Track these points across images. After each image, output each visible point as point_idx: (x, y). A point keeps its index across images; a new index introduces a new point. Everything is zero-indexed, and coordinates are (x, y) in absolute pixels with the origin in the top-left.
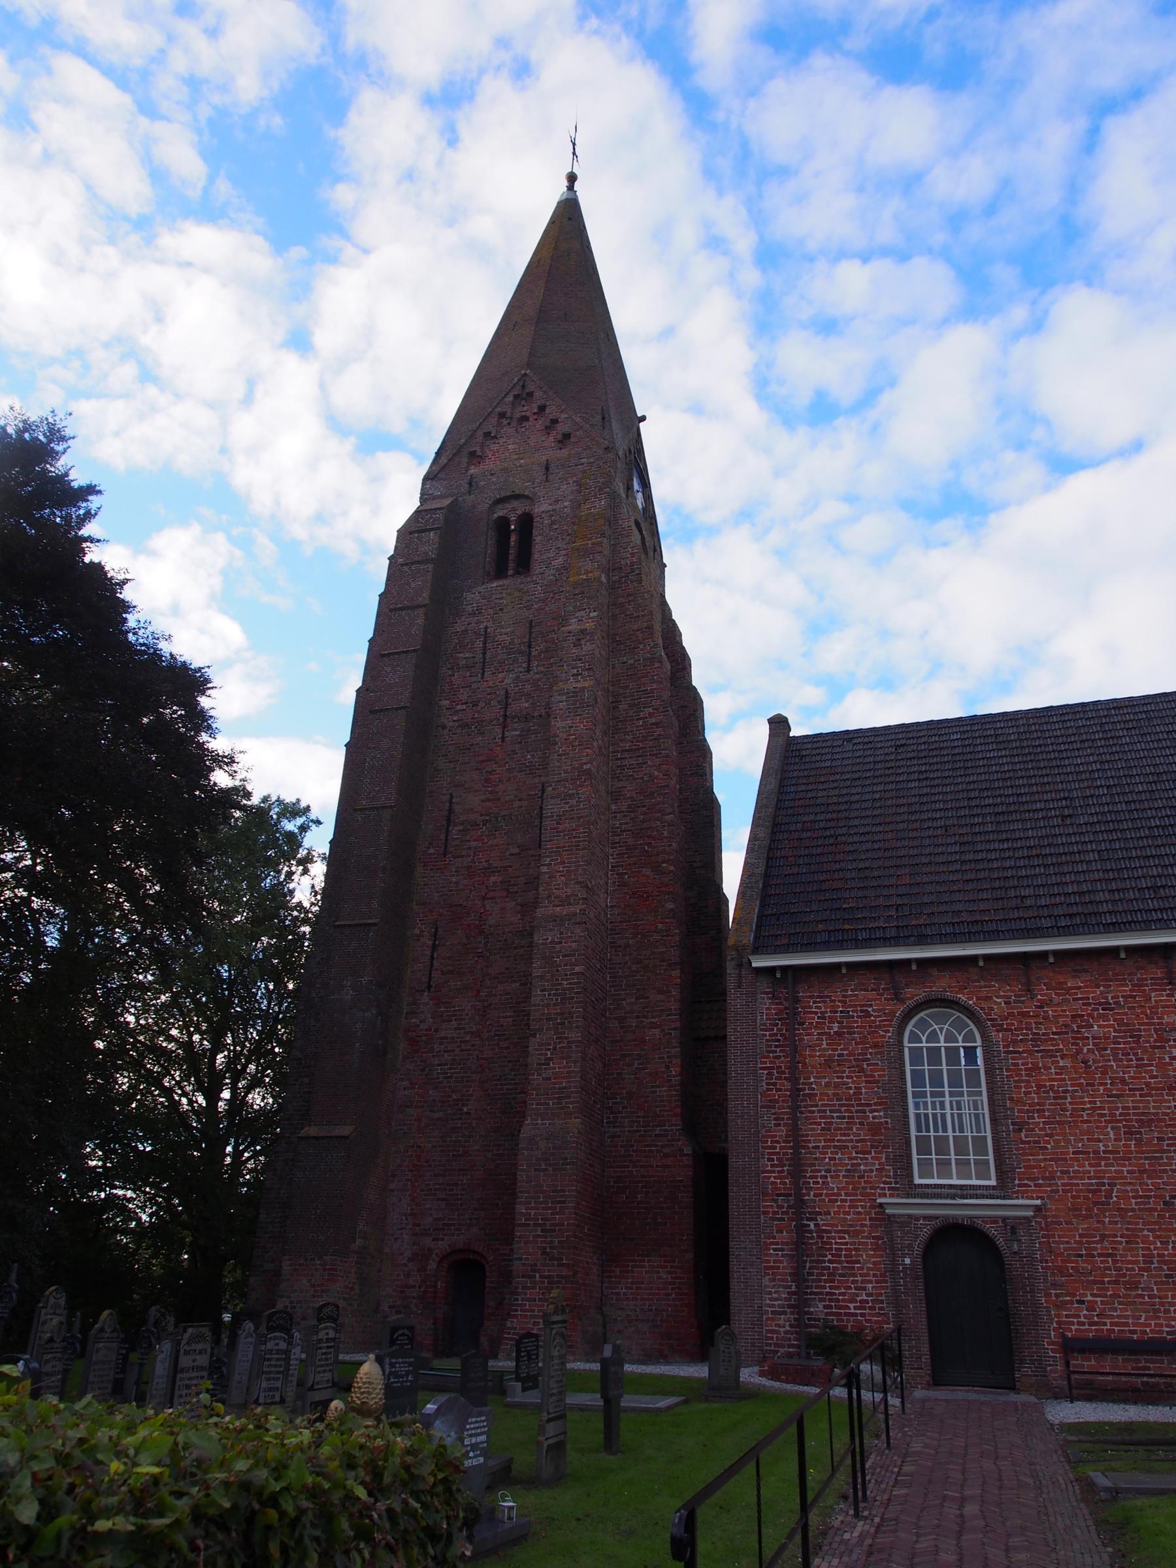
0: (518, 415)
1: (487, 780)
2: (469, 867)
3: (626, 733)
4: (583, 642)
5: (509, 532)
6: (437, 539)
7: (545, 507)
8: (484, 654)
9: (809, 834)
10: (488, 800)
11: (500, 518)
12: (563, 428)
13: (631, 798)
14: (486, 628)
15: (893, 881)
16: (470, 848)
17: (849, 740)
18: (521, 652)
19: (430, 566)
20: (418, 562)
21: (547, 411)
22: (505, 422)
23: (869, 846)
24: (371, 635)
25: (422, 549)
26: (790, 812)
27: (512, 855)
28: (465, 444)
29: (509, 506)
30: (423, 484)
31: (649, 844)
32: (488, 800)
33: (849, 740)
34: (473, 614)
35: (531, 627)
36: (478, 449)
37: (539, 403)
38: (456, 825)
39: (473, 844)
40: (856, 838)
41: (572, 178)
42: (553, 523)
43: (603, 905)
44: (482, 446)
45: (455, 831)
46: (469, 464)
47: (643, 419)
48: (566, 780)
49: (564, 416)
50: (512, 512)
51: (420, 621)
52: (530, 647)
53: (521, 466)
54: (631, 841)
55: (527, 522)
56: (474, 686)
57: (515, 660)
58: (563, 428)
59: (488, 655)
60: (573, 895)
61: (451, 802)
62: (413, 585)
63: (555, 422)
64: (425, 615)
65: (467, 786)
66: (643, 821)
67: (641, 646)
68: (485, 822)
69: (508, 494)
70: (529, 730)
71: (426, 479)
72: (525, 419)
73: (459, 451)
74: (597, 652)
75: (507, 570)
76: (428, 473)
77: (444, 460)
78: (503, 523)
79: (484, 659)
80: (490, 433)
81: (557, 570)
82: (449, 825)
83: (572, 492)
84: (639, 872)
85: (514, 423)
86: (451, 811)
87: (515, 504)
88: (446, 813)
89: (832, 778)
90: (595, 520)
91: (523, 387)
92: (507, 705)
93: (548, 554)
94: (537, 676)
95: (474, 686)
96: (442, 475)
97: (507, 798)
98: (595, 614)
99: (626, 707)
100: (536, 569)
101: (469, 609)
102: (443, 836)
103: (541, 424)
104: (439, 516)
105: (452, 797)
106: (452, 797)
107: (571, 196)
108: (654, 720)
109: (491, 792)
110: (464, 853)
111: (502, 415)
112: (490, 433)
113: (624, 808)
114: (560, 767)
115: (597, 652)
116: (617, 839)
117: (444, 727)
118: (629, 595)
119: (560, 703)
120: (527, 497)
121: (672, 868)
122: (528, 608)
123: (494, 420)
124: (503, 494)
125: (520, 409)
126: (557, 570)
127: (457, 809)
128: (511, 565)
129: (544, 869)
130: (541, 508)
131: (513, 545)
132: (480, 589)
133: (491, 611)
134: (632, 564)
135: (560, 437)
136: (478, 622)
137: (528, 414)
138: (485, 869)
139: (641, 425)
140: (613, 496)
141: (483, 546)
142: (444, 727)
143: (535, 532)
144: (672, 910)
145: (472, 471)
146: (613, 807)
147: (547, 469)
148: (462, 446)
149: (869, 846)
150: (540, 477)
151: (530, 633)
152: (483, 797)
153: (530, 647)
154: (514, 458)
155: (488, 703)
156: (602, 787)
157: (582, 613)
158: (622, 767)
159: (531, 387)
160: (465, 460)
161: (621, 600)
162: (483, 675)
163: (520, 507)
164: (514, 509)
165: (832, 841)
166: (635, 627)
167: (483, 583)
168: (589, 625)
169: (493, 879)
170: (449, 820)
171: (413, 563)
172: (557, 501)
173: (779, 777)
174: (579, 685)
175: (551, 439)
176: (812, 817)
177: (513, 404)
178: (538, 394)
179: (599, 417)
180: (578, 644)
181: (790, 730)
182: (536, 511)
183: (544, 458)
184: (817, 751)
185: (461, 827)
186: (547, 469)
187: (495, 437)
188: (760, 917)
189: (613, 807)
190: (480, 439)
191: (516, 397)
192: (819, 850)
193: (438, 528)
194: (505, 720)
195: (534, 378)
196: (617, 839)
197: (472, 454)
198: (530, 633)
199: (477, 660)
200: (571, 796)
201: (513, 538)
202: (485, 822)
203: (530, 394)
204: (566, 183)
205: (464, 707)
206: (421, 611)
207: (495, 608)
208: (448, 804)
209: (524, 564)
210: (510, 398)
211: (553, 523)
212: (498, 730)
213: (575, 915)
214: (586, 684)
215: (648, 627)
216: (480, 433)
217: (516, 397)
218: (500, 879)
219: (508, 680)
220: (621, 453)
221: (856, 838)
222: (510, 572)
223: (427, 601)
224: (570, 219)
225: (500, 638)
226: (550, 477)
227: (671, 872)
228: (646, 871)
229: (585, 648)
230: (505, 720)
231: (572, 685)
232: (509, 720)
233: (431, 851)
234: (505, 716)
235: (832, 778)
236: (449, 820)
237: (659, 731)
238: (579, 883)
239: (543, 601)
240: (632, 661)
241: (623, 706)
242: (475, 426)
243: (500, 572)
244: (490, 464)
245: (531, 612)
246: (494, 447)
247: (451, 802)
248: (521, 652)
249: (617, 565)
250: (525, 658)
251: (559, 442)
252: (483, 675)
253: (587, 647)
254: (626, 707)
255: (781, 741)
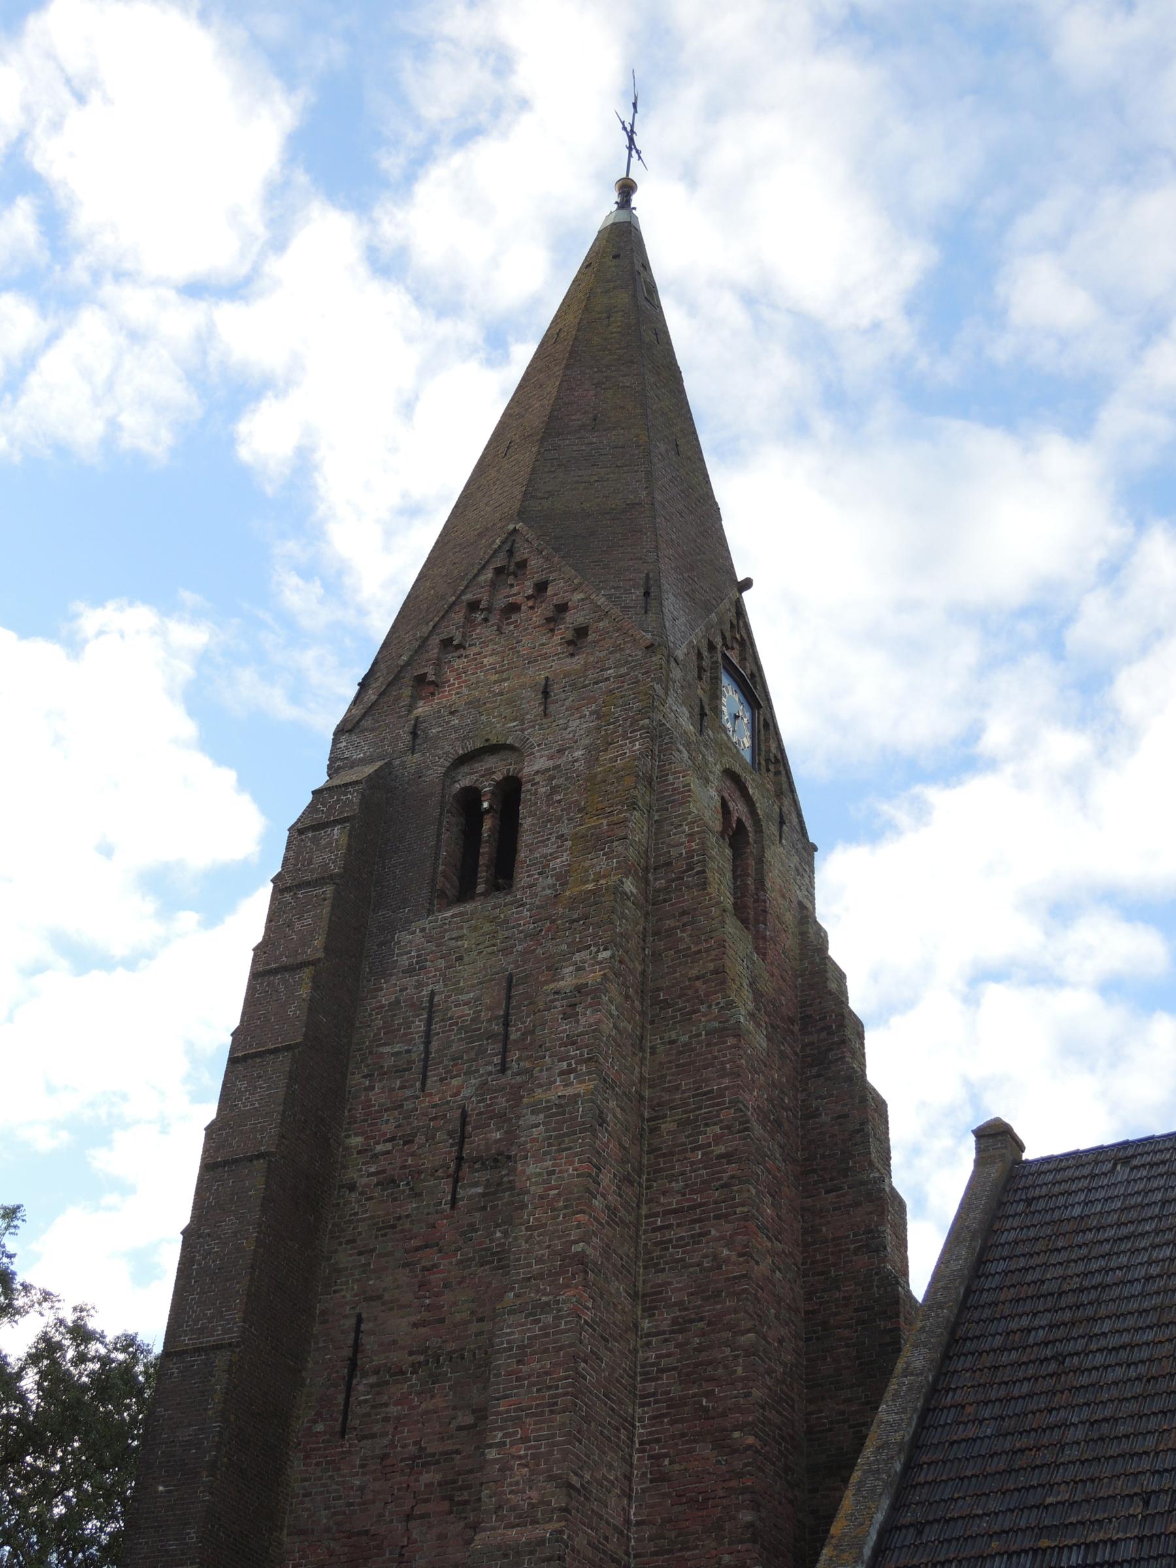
0: (500, 602)
1: (421, 1286)
2: (384, 1457)
3: (672, 1178)
4: (579, 1009)
5: (479, 815)
6: (344, 840)
7: (541, 763)
8: (427, 1043)
9: (1014, 1355)
10: (423, 1323)
11: (465, 790)
12: (574, 618)
13: (680, 1303)
14: (433, 994)
15: (1150, 1443)
16: (386, 1419)
17: (1126, 1161)
18: (491, 1036)
19: (329, 890)
20: (308, 884)
21: (550, 591)
22: (479, 616)
23: (1119, 1372)
24: (235, 1022)
25: (318, 860)
26: (987, 1313)
27: (460, 1428)
28: (407, 664)
29: (481, 766)
30: (335, 741)
31: (709, 1394)
32: (423, 1323)
33: (1126, 1161)
34: (410, 971)
35: (510, 987)
36: (430, 671)
37: (536, 578)
38: (365, 1375)
39: (394, 1410)
40: (1099, 1359)
41: (627, 189)
42: (554, 790)
43: (618, 1521)
44: (438, 664)
45: (362, 1386)
46: (415, 698)
47: (747, 584)
48: (539, 1276)
49: (578, 596)
50: (484, 777)
51: (304, 992)
52: (506, 1024)
53: (501, 694)
54: (676, 1391)
55: (510, 791)
56: (408, 1105)
57: (481, 1052)
58: (574, 618)
59: (435, 1045)
60: (542, 1502)
61: (358, 1331)
62: (298, 926)
63: (562, 608)
64: (314, 979)
65: (387, 1297)
66: (700, 1349)
67: (703, 1008)
68: (416, 1368)
69: (479, 745)
70: (499, 1184)
71: (341, 731)
72: (514, 608)
73: (397, 678)
74: (607, 1027)
75: (475, 885)
76: (344, 721)
77: (371, 696)
78: (471, 797)
79: (427, 1052)
80: (451, 639)
81: (558, 877)
82: (351, 1375)
83: (589, 732)
84: (689, 1451)
85: (494, 619)
86: (356, 1347)
87: (491, 762)
88: (347, 1352)
89: (1079, 1239)
90: (620, 779)
91: (511, 552)
92: (463, 1137)
93: (542, 847)
94: (519, 1079)
95: (408, 1105)
96: (367, 723)
97: (458, 1317)
98: (606, 954)
99: (673, 1126)
100: (522, 878)
101: (404, 961)
102: (340, 1398)
103: (537, 616)
104: (354, 797)
105: (360, 1320)
106: (360, 1320)
107: (623, 216)
108: (721, 1149)
109: (428, 1308)
110: (376, 1428)
111: (473, 606)
112: (451, 639)
113: (665, 1325)
114: (528, 1252)
115: (607, 1027)
116: (651, 1387)
117: (352, 1187)
118: (683, 913)
119: (534, 1128)
120: (511, 748)
121: (751, 1440)
122: (506, 951)
123: (458, 617)
124: (470, 746)
125: (506, 591)
126: (558, 877)
127: (369, 1342)
128: (483, 874)
129: (492, 1454)
130: (536, 764)
131: (484, 836)
132: (425, 923)
133: (442, 963)
134: (691, 853)
135: (569, 635)
136: (419, 985)
137: (518, 599)
138: (413, 1458)
139: (746, 595)
140: (660, 739)
141: (433, 842)
142: (352, 1187)
143: (523, 811)
144: (751, 1525)
145: (418, 711)
146: (646, 1324)
147: (546, 693)
148: (403, 668)
149: (1119, 1372)
150: (532, 707)
151: (509, 998)
152: (413, 1319)
153: (506, 1024)
154: (488, 680)
155: (430, 1137)
156: (618, 1287)
157: (584, 955)
158: (663, 1244)
159: (523, 552)
160: (407, 692)
161: (669, 923)
162: (424, 1084)
163: (499, 767)
164: (490, 772)
165: (1053, 1366)
166: (694, 972)
167: (430, 912)
168: (592, 977)
169: (426, 1478)
170: (353, 1365)
171: (299, 886)
172: (561, 751)
173: (978, 1244)
174: (569, 1091)
175: (557, 639)
176: (1025, 1322)
177: (493, 585)
178: (534, 563)
179: (640, 592)
180: (570, 1014)
181: (1021, 1147)
182: (526, 771)
183: (544, 674)
184: (1064, 1187)
185: (373, 1379)
186: (546, 693)
187: (460, 646)
188: (888, 1530)
189: (646, 1324)
190: (434, 652)
191: (499, 571)
192: (1026, 1388)
193: (346, 820)
194: (458, 1167)
195: (530, 536)
196: (651, 1387)
197: (421, 680)
198: (509, 998)
199: (414, 1056)
200: (545, 1307)
201: (488, 824)
202: (416, 1368)
203: (523, 565)
204: (615, 197)
205: (389, 1146)
206: (306, 974)
207: (446, 957)
208: (353, 1335)
209: (504, 872)
210: (488, 575)
211: (554, 790)
212: (446, 1186)
213: (541, 1542)
214: (580, 1089)
215: (716, 972)
216: (435, 641)
217: (499, 571)
218: (438, 1477)
219: (465, 1088)
220: (680, 653)
221: (1099, 1359)
222: (481, 888)
223: (320, 954)
224: (616, 257)
225: (455, 1011)
226: (552, 708)
227: (749, 1447)
228: (704, 1449)
229: (583, 1020)
230: (458, 1167)
231: (560, 1090)
232: (465, 1166)
233: (320, 1427)
234: (460, 1159)
235: (1079, 1239)
236: (353, 1365)
237: (732, 1169)
238: (551, 1478)
239: (534, 936)
240: (685, 1038)
241: (667, 1126)
242: (426, 630)
243: (465, 893)
244: (450, 696)
245: (511, 958)
246: (459, 664)
247: (358, 1331)
248: (491, 1036)
249: (662, 859)
250: (498, 1047)
251: (570, 643)
252: (424, 1084)
253: (587, 1018)
254: (673, 1126)
255: (995, 1171)
